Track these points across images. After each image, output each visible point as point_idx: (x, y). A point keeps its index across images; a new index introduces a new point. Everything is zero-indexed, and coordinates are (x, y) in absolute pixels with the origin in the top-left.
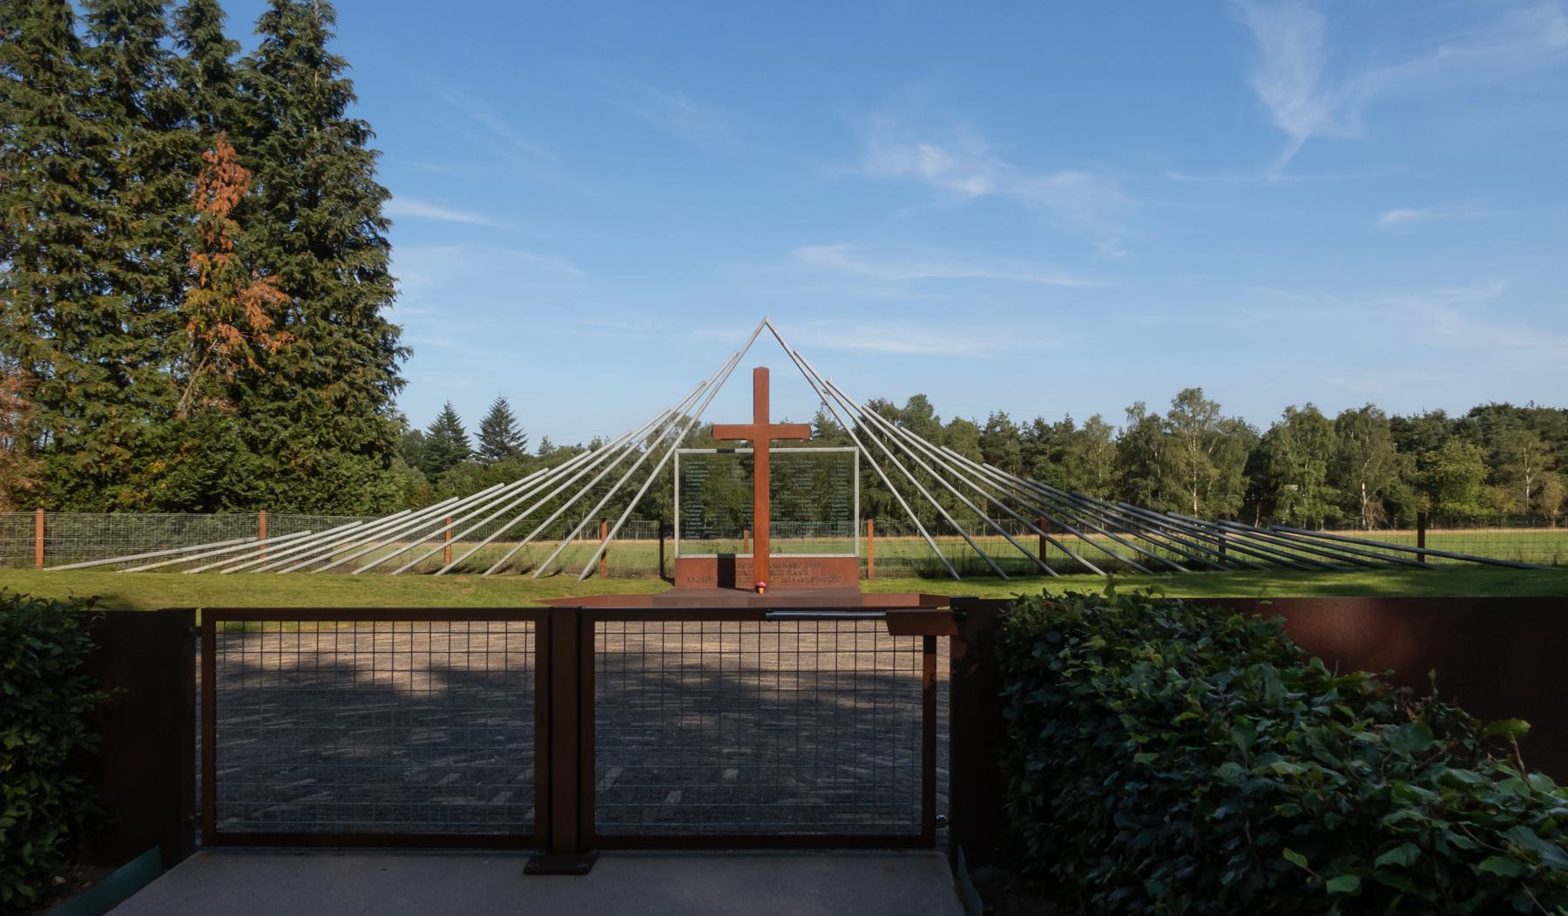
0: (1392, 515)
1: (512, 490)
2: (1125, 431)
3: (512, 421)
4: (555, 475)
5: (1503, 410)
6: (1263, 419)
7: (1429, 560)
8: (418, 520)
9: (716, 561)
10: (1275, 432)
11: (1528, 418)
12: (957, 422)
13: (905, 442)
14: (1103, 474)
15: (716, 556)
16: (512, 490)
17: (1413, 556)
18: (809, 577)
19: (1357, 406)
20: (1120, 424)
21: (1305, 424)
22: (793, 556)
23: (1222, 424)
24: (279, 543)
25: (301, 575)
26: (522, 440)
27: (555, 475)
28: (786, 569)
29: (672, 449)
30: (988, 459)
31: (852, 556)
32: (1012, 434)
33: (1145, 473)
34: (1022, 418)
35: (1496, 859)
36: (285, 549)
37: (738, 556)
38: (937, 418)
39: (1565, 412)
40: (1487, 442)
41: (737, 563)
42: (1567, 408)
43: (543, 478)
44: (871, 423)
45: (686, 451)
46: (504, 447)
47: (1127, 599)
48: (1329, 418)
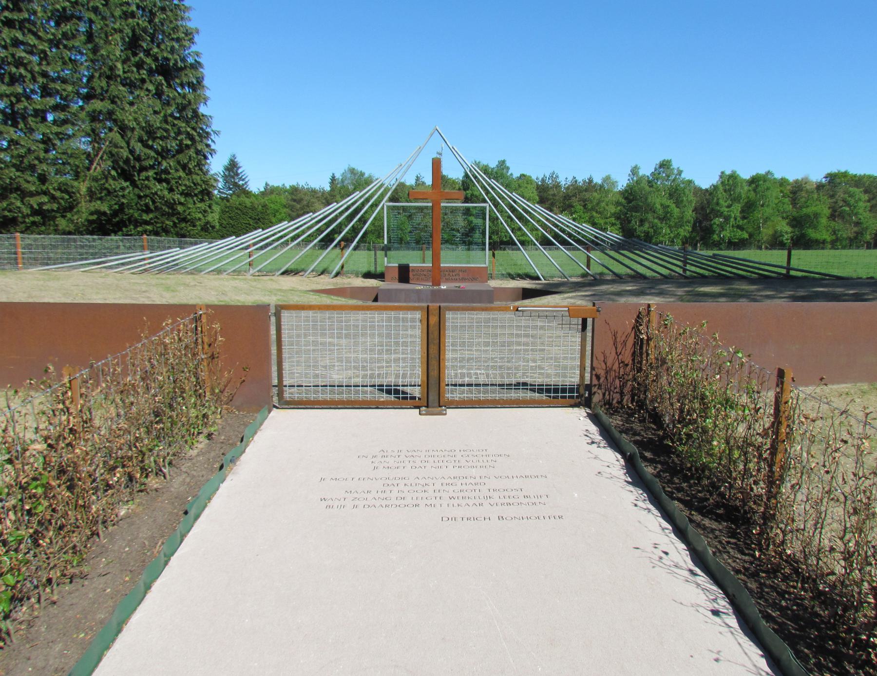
0: (776, 243)
1: (292, 226)
2: (625, 185)
3: (240, 167)
4: (316, 217)
5: (845, 174)
6: (706, 179)
7: (792, 273)
8: (239, 243)
9: (397, 270)
10: (715, 187)
11: (858, 181)
12: (523, 176)
13: (493, 188)
14: (612, 209)
15: (397, 265)
16: (292, 226)
17: (784, 271)
18: (461, 277)
19: (762, 172)
20: (622, 182)
21: (730, 182)
22: (452, 265)
23: (683, 182)
24: (164, 254)
25: (104, 270)
26: (246, 180)
27: (316, 217)
28: (447, 273)
29: (382, 203)
30: (542, 202)
31: (484, 266)
32: (557, 186)
33: (636, 209)
34: (565, 179)
35: (598, 253)
36: (168, 258)
37: (411, 265)
38: (512, 174)
39: (872, 179)
40: (832, 196)
41: (410, 269)
42: (876, 174)
43: (310, 219)
44: (482, 184)
45: (391, 204)
46: (236, 185)
47: (692, 185)
48: (744, 178)
